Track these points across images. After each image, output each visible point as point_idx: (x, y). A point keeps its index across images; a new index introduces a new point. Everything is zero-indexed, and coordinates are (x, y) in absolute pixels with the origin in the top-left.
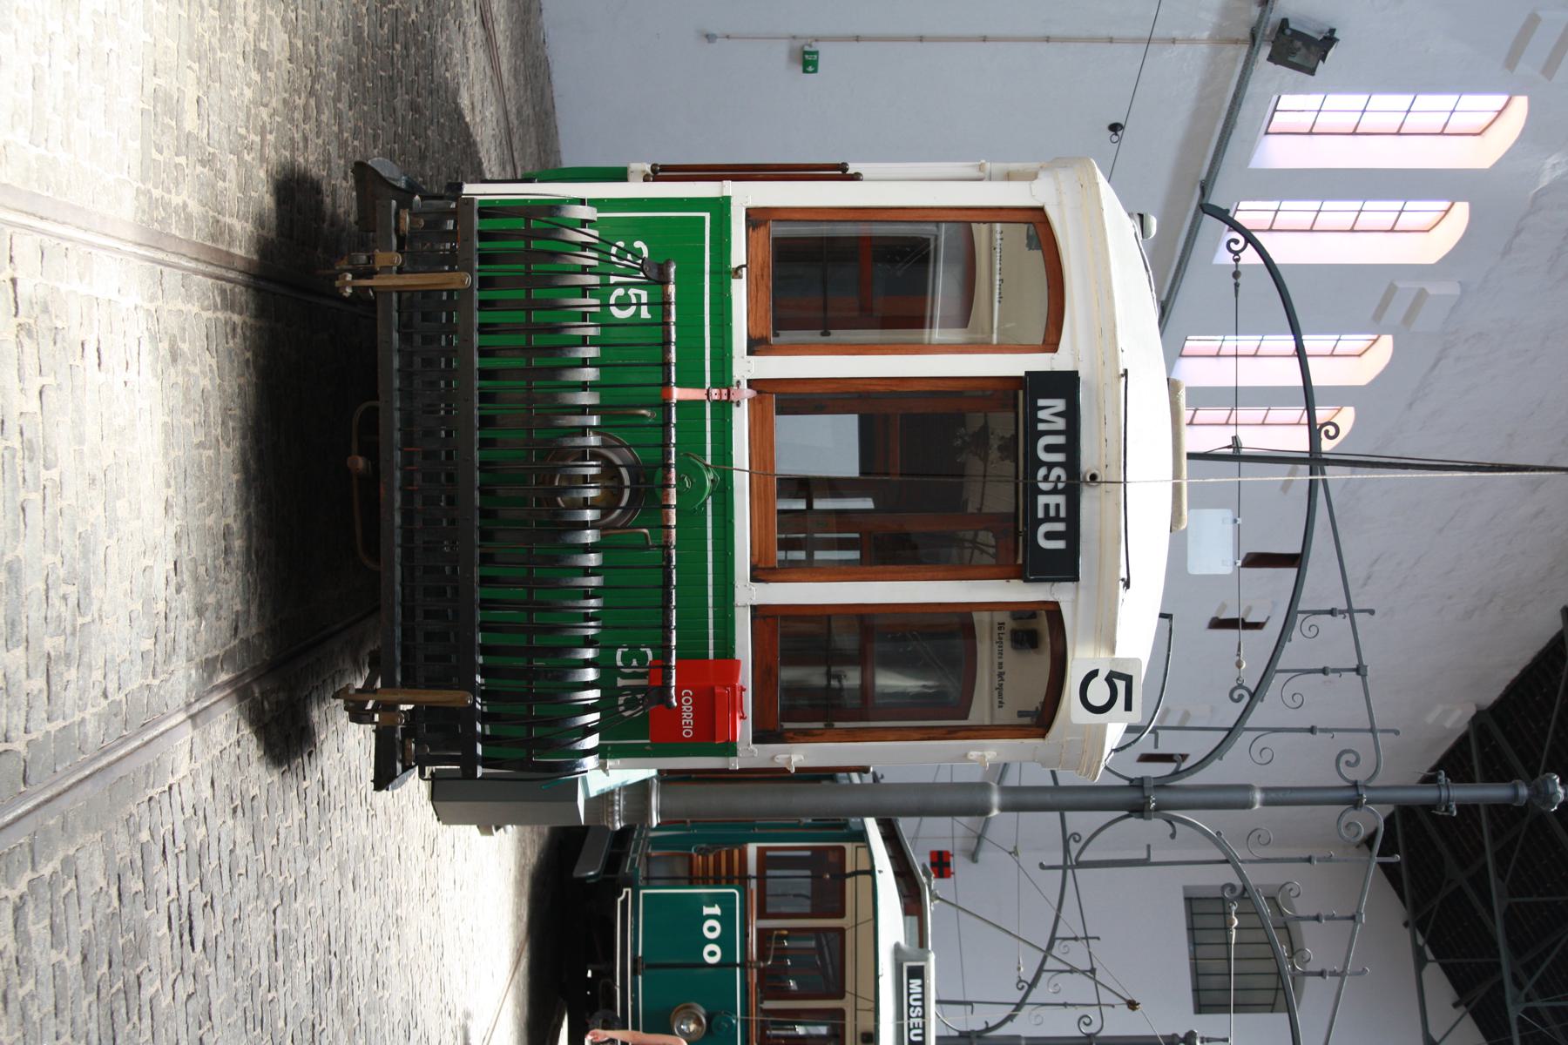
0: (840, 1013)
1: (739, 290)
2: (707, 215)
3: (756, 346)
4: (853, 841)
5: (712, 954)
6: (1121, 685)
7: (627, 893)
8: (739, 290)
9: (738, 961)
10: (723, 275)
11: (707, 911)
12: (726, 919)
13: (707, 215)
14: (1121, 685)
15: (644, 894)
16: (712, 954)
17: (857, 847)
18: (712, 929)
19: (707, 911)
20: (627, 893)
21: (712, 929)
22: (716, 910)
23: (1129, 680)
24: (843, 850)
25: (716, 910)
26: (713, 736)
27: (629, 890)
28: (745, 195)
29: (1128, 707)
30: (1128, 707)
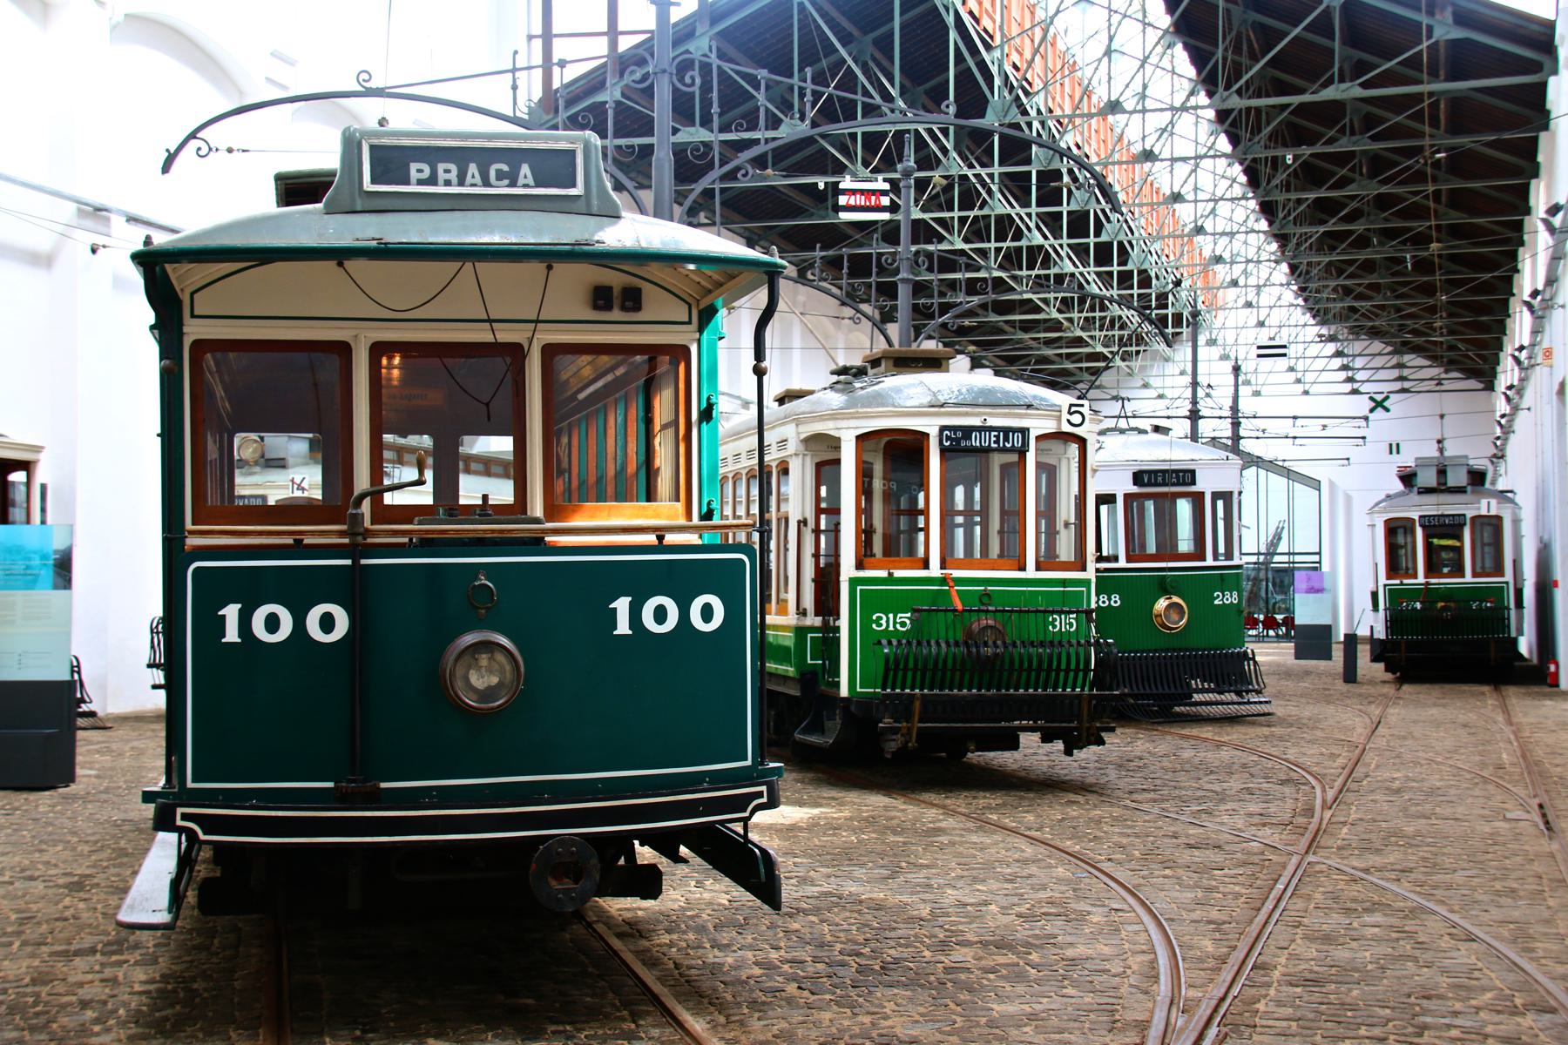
0: (551, 352)
1: (898, 573)
2: (859, 588)
3: (1023, 568)
4: (181, 324)
5: (327, 623)
6: (1073, 409)
7: (185, 817)
8: (898, 573)
9: (348, 562)
10: (891, 580)
11: (232, 635)
12: (251, 591)
13: (859, 588)
14: (1073, 409)
15: (194, 781)
16: (327, 623)
17: (193, 316)
18: (272, 623)
19: (232, 635)
20: (185, 817)
21: (272, 623)
22: (231, 612)
23: (1071, 405)
24: (200, 346)
25: (231, 612)
26: (1087, 583)
27: (180, 811)
28: (848, 569)
29: (1082, 406)
30: (1082, 406)
